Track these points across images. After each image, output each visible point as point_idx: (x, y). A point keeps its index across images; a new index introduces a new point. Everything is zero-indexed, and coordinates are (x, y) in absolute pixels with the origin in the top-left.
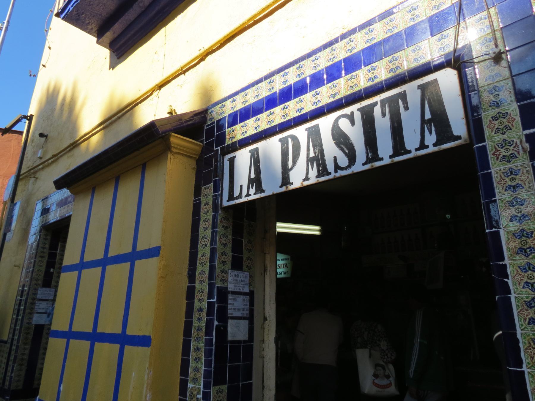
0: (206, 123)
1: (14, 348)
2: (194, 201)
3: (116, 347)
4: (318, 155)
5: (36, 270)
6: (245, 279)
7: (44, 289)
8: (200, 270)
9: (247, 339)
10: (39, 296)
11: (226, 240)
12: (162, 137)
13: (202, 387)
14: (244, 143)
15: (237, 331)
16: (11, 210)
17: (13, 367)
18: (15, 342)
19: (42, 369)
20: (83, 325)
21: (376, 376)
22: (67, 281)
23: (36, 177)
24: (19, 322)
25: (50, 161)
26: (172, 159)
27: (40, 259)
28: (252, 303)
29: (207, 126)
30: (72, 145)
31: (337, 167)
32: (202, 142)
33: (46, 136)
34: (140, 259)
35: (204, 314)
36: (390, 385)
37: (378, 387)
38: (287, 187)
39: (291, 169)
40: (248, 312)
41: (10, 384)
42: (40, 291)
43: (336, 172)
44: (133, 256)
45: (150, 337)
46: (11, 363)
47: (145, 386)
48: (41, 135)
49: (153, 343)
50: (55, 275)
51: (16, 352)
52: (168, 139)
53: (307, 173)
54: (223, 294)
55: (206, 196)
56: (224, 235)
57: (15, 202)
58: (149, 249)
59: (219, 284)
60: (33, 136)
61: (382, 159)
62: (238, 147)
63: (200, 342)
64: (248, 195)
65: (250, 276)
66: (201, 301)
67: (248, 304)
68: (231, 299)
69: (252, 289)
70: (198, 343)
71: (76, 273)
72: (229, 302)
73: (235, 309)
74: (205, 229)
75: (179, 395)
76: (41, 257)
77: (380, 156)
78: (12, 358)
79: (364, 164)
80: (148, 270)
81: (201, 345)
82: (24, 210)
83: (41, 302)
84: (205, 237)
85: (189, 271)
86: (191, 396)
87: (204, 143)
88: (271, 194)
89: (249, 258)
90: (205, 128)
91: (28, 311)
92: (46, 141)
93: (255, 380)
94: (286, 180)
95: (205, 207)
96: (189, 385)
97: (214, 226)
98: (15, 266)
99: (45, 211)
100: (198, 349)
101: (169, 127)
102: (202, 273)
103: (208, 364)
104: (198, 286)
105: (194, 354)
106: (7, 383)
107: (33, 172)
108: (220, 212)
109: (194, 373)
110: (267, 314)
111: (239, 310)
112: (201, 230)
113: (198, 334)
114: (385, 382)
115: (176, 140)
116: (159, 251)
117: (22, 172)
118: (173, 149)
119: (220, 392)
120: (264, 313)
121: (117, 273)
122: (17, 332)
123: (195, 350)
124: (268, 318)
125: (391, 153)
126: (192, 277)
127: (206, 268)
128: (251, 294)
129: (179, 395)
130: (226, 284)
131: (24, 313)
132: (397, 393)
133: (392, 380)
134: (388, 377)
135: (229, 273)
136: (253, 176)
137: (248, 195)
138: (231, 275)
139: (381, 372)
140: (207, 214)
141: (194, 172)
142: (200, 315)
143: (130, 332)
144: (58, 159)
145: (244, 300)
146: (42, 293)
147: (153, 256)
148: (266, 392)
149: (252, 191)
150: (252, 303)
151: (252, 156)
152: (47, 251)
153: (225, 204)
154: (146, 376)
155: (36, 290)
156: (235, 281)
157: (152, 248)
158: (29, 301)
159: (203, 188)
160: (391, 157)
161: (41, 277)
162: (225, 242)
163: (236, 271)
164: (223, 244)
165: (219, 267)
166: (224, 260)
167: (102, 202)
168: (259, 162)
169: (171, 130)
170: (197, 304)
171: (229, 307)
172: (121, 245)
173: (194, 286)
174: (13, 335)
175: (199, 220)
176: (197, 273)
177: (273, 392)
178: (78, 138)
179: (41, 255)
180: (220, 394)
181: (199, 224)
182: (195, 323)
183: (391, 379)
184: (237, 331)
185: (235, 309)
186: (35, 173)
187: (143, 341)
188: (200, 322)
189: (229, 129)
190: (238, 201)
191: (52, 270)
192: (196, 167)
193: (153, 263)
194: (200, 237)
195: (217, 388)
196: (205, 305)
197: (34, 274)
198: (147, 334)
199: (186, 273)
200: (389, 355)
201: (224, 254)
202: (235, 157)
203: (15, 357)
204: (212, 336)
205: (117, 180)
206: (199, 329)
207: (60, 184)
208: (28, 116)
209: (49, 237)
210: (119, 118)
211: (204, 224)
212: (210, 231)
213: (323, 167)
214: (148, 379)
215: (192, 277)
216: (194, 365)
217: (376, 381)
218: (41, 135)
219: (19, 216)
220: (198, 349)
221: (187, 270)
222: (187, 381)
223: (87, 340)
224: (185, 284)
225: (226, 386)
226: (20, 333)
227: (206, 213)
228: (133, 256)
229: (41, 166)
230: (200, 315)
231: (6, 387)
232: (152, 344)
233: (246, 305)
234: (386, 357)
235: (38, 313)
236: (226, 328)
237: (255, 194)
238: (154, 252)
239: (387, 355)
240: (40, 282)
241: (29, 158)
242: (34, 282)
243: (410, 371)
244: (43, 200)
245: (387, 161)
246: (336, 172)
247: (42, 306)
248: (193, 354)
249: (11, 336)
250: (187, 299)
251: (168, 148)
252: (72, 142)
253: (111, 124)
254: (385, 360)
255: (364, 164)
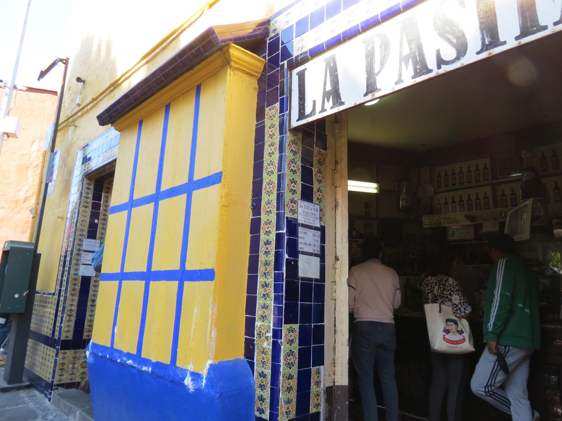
0: (268, 37)
1: (62, 298)
2: (257, 125)
3: (175, 284)
4: (415, 52)
5: (80, 220)
6: (315, 213)
7: (89, 240)
8: (266, 200)
9: (319, 278)
10: (84, 248)
11: (295, 166)
12: (221, 49)
13: (272, 324)
14: (316, 52)
15: (308, 268)
16: (52, 160)
17: (62, 317)
18: (63, 293)
19: (91, 321)
20: (136, 264)
21: (447, 331)
22: (115, 223)
23: (76, 125)
24: (66, 273)
25: (89, 107)
26: (232, 75)
27: (84, 209)
28: (323, 240)
29: (270, 39)
30: (112, 85)
31: (440, 62)
32: (264, 57)
33: (84, 82)
34: (198, 189)
35: (272, 248)
36: (463, 340)
37: (449, 343)
38: (373, 95)
39: (378, 73)
40: (319, 249)
41: (60, 334)
42: (85, 241)
43: (439, 67)
44: (190, 187)
45: (213, 270)
46: (60, 314)
47: (210, 322)
48: (79, 80)
49: (217, 276)
50: (100, 226)
51: (65, 302)
52: (228, 51)
53: (400, 75)
54: (293, 226)
55: (271, 118)
56: (293, 161)
57: (55, 151)
58: (209, 177)
59: (288, 214)
60: (70, 80)
61: (505, 43)
62: (310, 57)
63: (268, 277)
64: (323, 110)
65: (321, 210)
66: (268, 233)
67: (319, 240)
68: (301, 232)
69: (323, 224)
70: (266, 278)
71: (125, 213)
72: (300, 235)
73: (305, 244)
74: (270, 154)
75: (246, 335)
76: (84, 206)
77: (502, 39)
78: (60, 308)
79: (478, 53)
80: (207, 200)
81: (270, 280)
82: (64, 160)
83: (87, 253)
84: (272, 163)
85: (252, 202)
86: (260, 334)
87: (267, 58)
88: (352, 105)
89: (319, 190)
90: (268, 42)
91: (74, 262)
92: (84, 87)
93: (327, 323)
94: (371, 88)
95: (270, 130)
96: (256, 323)
97: (281, 149)
98: (58, 217)
99: (86, 160)
100: (266, 285)
101: (229, 36)
102: (269, 203)
103: (277, 299)
104: (264, 217)
105: (261, 290)
106: (57, 333)
107: (72, 120)
108: (288, 134)
109: (262, 310)
110: (339, 254)
111: (310, 245)
112: (266, 156)
113: (266, 269)
114: (458, 337)
115: (237, 53)
116: (220, 177)
117: (60, 122)
118: (233, 64)
119: (291, 330)
120: (336, 253)
121: (172, 208)
122: (64, 283)
123: (263, 286)
124: (340, 258)
125: (518, 33)
126: (256, 208)
127: (274, 197)
128: (322, 229)
129: (246, 335)
130: (296, 215)
131: (70, 264)
132: (472, 349)
133: (466, 335)
134: (461, 332)
135: (299, 204)
136: (329, 88)
137: (323, 110)
138: (301, 207)
139: (453, 327)
140: (272, 138)
141: (256, 93)
142: (267, 249)
143: (189, 267)
144: (97, 104)
145: (315, 236)
146: (88, 244)
147: (214, 183)
148: (338, 336)
149: (328, 105)
150: (323, 240)
151: (328, 64)
152: (90, 201)
153: (295, 123)
154: (210, 311)
155: (81, 240)
156: (305, 213)
157: (211, 176)
158: (75, 252)
159: (267, 109)
160: (517, 38)
161: (86, 228)
162: (294, 169)
163: (306, 203)
164: (292, 170)
165: (288, 196)
166: (293, 189)
167: (152, 133)
168: (336, 71)
169: (231, 40)
170: (263, 237)
171: (300, 240)
172: (175, 177)
173: (260, 218)
174: (61, 286)
175: (263, 145)
176: (263, 203)
177: (347, 336)
178: (118, 78)
179: (85, 204)
180: (291, 333)
181: (264, 149)
182: (262, 258)
183: (464, 334)
184: (308, 268)
185: (305, 244)
186: (74, 121)
187: (206, 275)
188: (267, 257)
189: (298, 38)
190: (310, 119)
191: (96, 221)
192: (257, 86)
193: (214, 190)
194: (265, 164)
195: (288, 326)
196: (272, 237)
197: (79, 224)
198: (210, 267)
199: (250, 204)
200: (462, 310)
201: (293, 181)
202: (305, 69)
203: (64, 308)
204: (281, 269)
205: (168, 108)
206: (267, 264)
207: (104, 119)
208: (64, 59)
209: (92, 187)
210: (164, 49)
211: (269, 148)
212: (277, 155)
213: (421, 65)
214: (212, 314)
215: (256, 208)
216: (261, 302)
217: (447, 336)
218: (79, 80)
219: (60, 167)
220: (266, 285)
221: (251, 201)
222: (254, 319)
223: (142, 280)
224: (250, 216)
225: (298, 325)
226: (67, 284)
227: (271, 136)
228: (190, 187)
229: (80, 114)
230: (267, 249)
231: (56, 338)
232: (215, 278)
233: (317, 241)
234: (459, 311)
235: (84, 264)
236: (296, 262)
237: (331, 108)
238: (215, 179)
239: (460, 309)
240: (85, 233)
241: (67, 107)
242: (78, 233)
243: (489, 324)
244: (84, 148)
245: (512, 44)
246: (439, 67)
247: (87, 258)
248: (260, 290)
249: (58, 287)
250: (251, 233)
251: (227, 62)
252: (112, 82)
253: (155, 56)
254: (458, 315)
255: (478, 53)
